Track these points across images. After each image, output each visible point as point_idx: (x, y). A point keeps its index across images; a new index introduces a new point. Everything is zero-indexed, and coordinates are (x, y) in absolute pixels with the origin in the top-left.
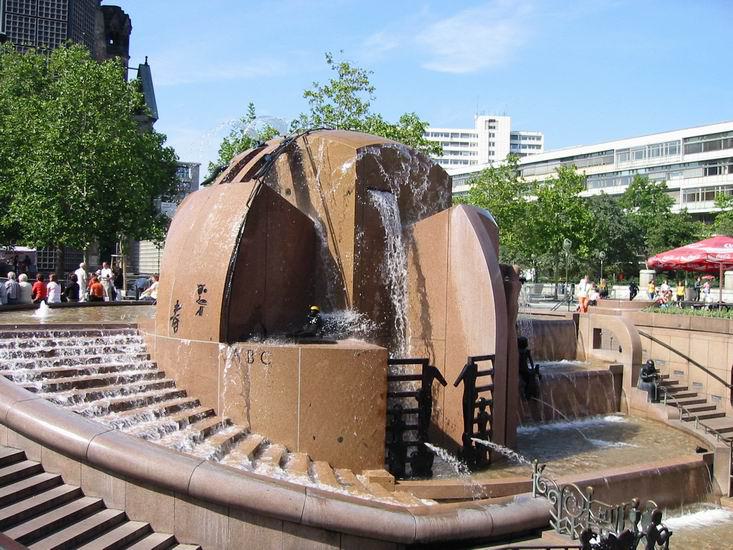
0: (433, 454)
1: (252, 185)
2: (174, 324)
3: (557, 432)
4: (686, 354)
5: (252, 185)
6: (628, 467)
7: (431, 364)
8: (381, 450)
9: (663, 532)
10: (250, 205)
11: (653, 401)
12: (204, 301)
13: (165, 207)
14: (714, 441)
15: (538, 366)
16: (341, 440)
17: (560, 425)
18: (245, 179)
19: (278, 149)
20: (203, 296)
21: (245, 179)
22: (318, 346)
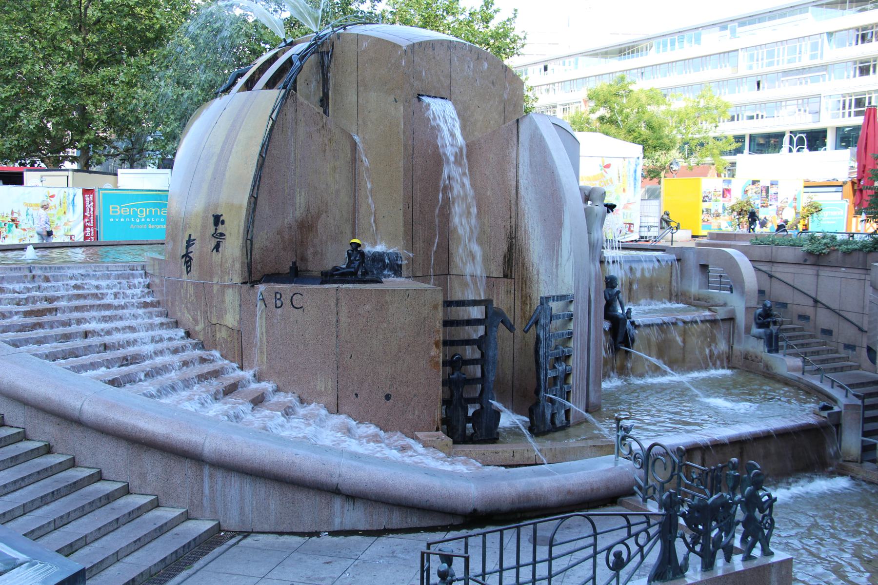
0: (492, 404)
1: (275, 94)
2: (186, 262)
3: (652, 387)
4: (791, 283)
5: (275, 94)
6: (737, 426)
7: (495, 305)
8: (439, 412)
9: (766, 498)
11: (769, 351)
12: (222, 234)
13: (709, 443)
14: (842, 399)
15: (629, 309)
16: (388, 397)
17: (650, 380)
18: (270, 85)
19: (307, 49)
20: (221, 228)
21: (270, 85)
22: (358, 286)
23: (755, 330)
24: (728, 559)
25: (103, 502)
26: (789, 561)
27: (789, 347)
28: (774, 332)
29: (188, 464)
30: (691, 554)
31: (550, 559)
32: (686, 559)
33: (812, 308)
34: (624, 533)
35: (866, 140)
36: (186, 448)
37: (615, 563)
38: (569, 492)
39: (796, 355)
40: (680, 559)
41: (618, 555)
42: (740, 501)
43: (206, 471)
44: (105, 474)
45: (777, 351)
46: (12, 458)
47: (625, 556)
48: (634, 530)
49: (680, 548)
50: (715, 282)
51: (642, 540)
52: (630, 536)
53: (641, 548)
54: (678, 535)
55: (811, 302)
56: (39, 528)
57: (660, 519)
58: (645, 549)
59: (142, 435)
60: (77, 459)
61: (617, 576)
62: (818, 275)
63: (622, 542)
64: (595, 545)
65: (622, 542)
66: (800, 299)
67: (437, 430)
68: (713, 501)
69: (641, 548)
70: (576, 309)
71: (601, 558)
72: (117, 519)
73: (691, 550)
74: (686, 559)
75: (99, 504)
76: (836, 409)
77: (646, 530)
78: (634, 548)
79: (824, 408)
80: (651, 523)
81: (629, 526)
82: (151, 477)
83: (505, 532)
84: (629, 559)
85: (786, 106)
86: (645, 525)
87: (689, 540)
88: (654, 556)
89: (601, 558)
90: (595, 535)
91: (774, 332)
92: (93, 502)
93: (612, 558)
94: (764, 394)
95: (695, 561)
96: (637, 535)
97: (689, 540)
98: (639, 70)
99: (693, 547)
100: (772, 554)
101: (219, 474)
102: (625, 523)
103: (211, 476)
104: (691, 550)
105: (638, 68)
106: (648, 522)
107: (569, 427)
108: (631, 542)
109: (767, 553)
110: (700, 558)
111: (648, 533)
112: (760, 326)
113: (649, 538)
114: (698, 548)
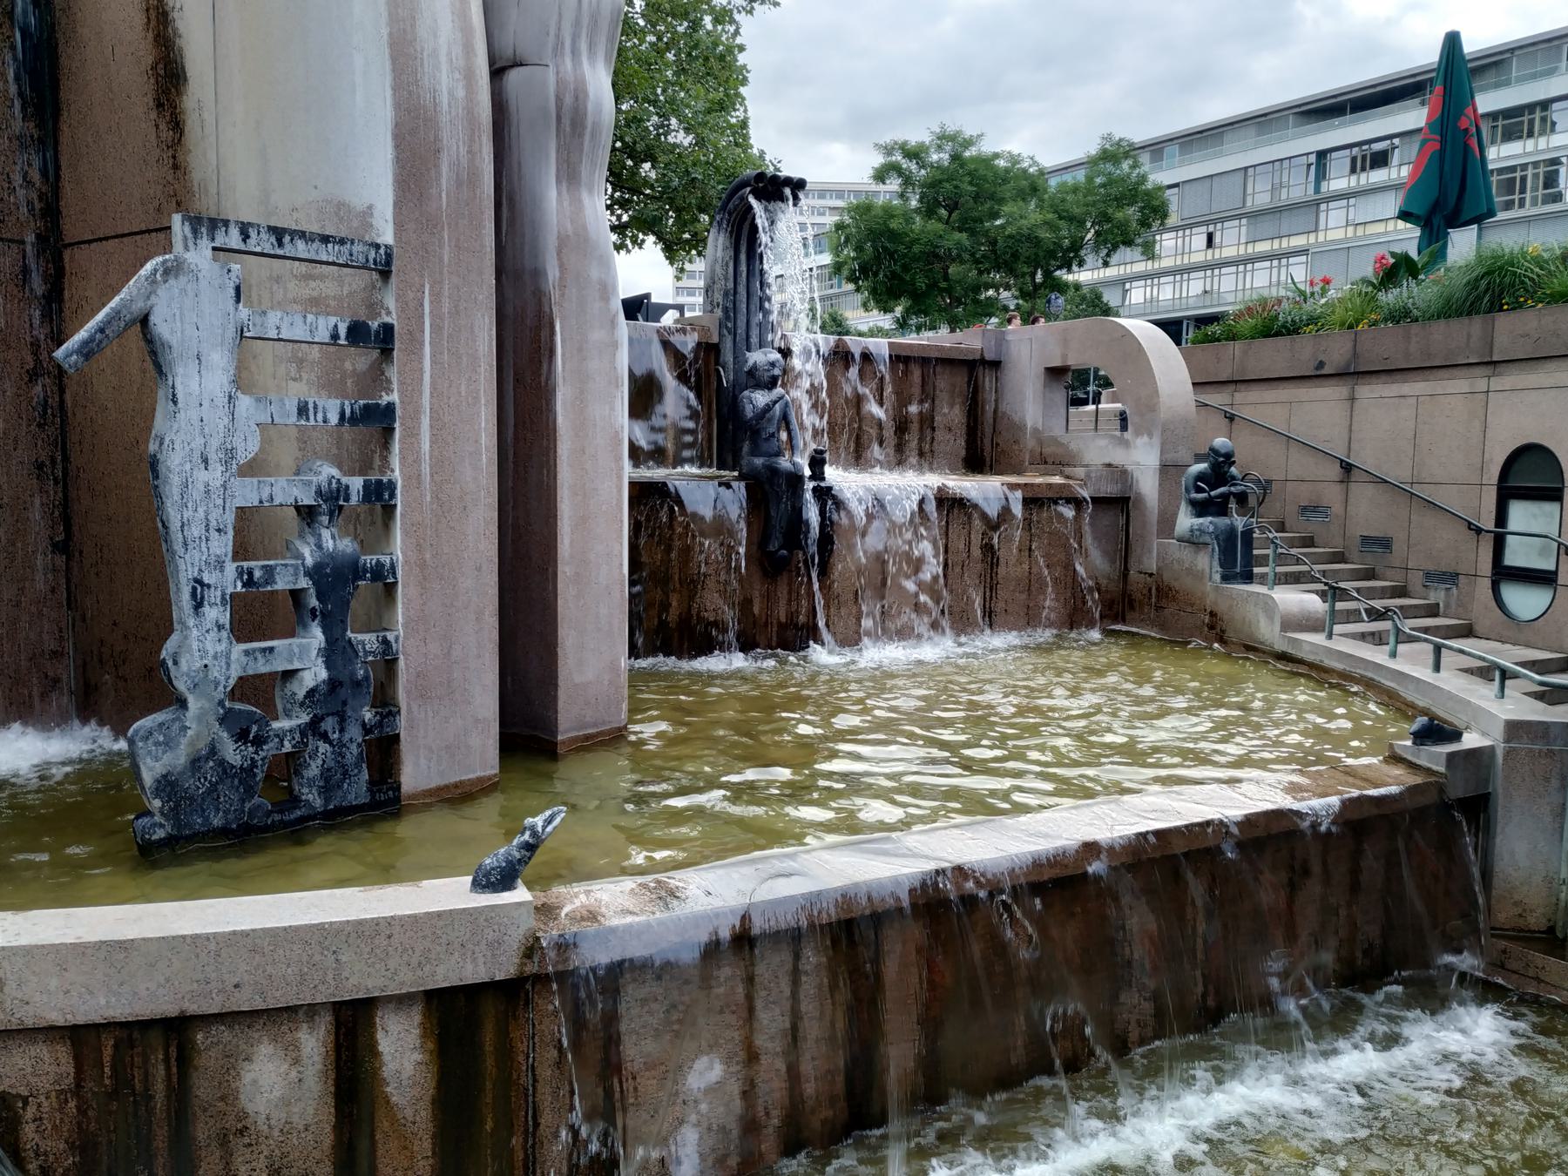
11: (1226, 578)
23: (1186, 521)
45: (1248, 577)
55: (1335, 471)
66: (1300, 465)
76: (1470, 740)
112: (1200, 509)
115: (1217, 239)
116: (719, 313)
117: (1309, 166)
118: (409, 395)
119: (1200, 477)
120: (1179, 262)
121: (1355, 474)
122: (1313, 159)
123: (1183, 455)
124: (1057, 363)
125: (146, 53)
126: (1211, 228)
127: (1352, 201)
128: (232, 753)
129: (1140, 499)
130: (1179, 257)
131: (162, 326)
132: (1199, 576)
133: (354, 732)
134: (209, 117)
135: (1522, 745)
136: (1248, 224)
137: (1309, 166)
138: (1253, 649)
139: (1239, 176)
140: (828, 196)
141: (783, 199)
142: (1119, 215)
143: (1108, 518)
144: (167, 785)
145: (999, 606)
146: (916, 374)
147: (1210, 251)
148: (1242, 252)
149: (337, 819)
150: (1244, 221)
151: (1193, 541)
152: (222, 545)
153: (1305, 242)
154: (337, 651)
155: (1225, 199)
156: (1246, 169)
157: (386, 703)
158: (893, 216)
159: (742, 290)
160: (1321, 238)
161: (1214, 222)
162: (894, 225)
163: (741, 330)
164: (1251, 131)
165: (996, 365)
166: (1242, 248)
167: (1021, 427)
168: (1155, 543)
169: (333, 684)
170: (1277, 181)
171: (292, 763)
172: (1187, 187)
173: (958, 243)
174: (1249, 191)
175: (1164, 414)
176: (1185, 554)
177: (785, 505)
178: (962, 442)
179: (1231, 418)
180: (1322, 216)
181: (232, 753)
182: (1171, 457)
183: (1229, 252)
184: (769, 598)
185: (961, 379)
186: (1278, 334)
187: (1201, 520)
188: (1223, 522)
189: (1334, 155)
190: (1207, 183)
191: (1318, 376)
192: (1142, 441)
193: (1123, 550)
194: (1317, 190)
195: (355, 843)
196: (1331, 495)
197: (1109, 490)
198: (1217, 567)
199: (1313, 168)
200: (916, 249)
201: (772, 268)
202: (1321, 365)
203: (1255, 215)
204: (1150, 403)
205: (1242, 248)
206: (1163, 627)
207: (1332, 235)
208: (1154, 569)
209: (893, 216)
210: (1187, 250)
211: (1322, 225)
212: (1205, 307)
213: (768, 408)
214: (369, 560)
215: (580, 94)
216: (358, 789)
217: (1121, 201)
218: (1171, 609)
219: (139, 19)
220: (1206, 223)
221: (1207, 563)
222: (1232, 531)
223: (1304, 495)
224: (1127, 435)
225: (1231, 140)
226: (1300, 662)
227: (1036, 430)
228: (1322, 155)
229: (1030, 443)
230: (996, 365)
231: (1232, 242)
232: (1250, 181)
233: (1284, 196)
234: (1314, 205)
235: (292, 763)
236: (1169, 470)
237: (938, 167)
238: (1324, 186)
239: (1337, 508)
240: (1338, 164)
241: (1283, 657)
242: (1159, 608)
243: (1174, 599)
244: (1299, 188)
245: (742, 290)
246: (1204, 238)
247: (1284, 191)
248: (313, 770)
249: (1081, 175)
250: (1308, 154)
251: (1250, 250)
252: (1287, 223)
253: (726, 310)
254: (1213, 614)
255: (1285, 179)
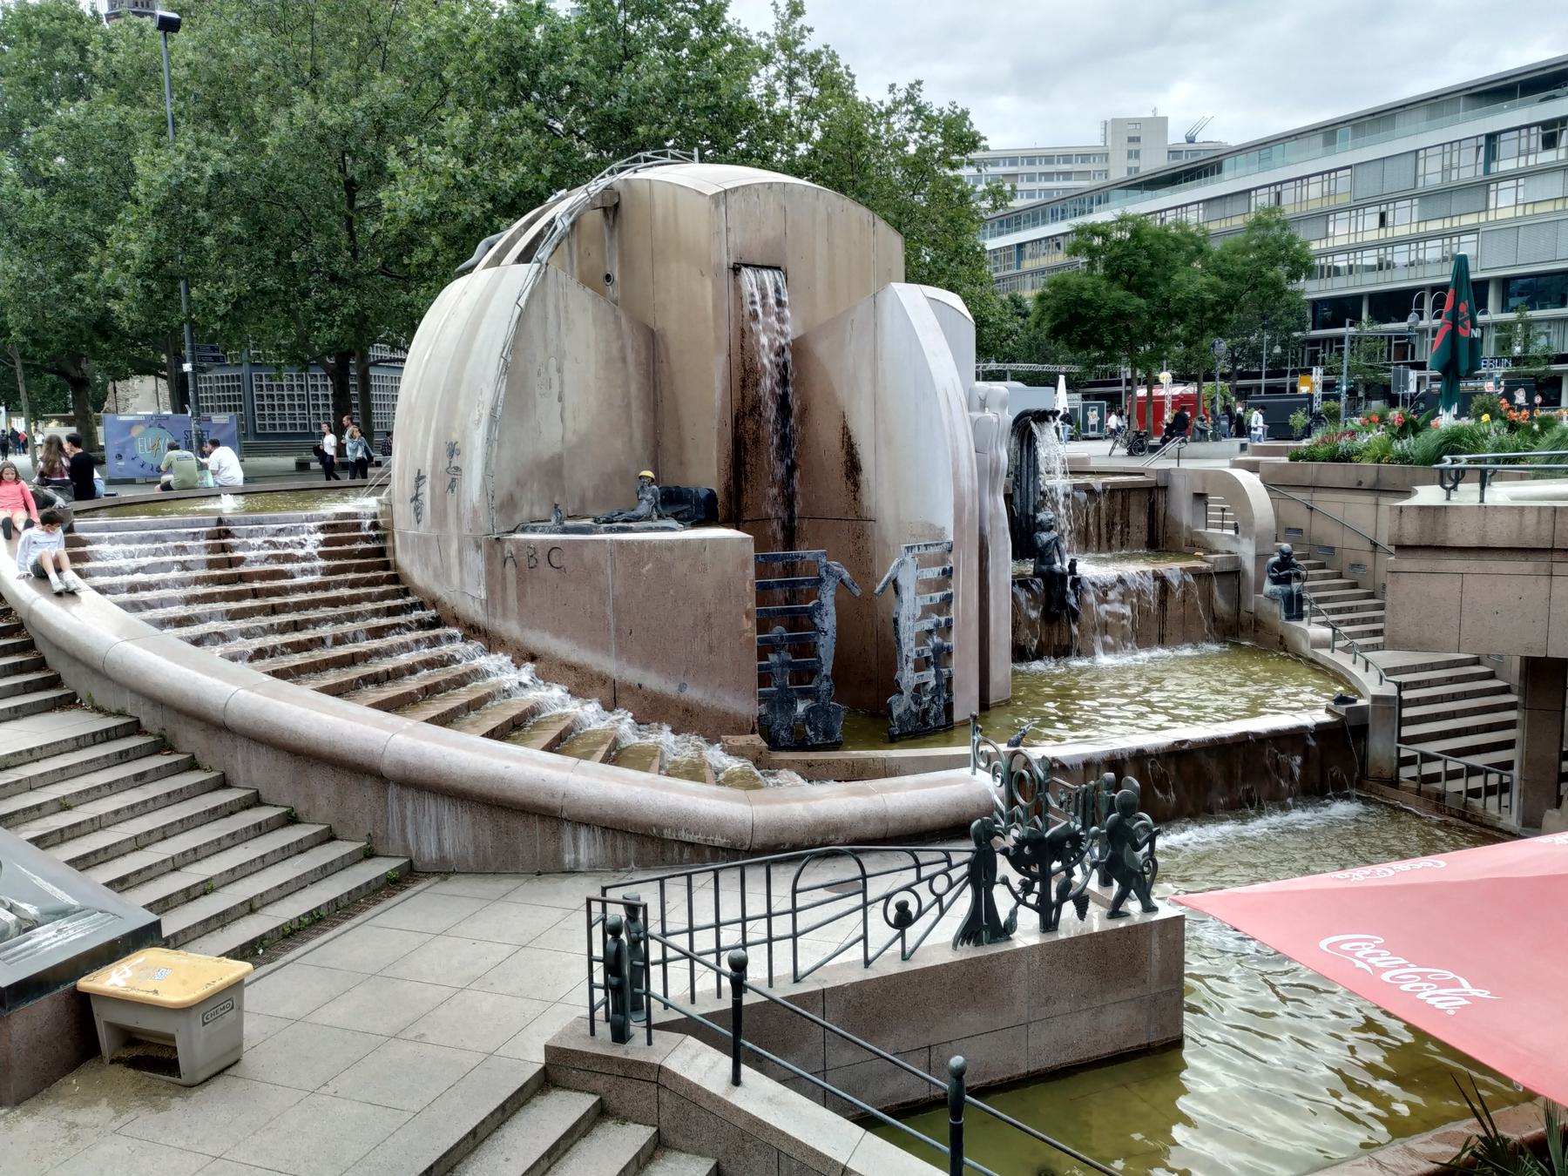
2: (416, 509)
10: (522, 302)
11: (1288, 618)
12: (457, 469)
20: (456, 462)
23: (1268, 587)
24: (1082, 912)
25: (252, 833)
26: (1179, 920)
27: (1318, 613)
28: (1295, 591)
29: (368, 782)
30: (1021, 908)
31: (794, 911)
32: (1013, 913)
33: (1370, 554)
34: (911, 876)
35: (178, 499)
36: (359, 760)
37: (898, 918)
38: (919, 820)
39: (1324, 624)
40: (1003, 916)
41: (902, 907)
42: (1095, 836)
43: (393, 791)
44: (264, 795)
45: (1300, 617)
46: (139, 774)
47: (913, 908)
48: (925, 872)
49: (1003, 901)
50: (1215, 517)
51: (941, 884)
52: (919, 880)
53: (939, 898)
54: (998, 879)
55: (1368, 546)
56: (149, 868)
57: (968, 856)
58: (946, 900)
59: (302, 744)
60: (228, 775)
61: (902, 935)
62: (1377, 505)
63: (908, 888)
64: (864, 892)
65: (908, 888)
66: (1350, 541)
67: (753, 732)
68: (1053, 834)
69: (939, 898)
70: (957, 561)
71: (875, 912)
72: (263, 857)
73: (1021, 902)
74: (1013, 913)
75: (244, 836)
76: (1361, 702)
77: (945, 872)
78: (928, 899)
79: (1341, 700)
80: (954, 863)
81: (918, 866)
82: (321, 801)
83: (722, 875)
84: (920, 913)
85: (1459, 244)
86: (945, 865)
87: (1017, 887)
88: (962, 906)
89: (875, 912)
90: (864, 877)
91: (1295, 591)
92: (235, 833)
93: (892, 913)
94: (1126, 686)
95: (1028, 920)
96: (931, 878)
97: (1017, 887)
98: (1272, 188)
99: (1024, 898)
100: (1155, 909)
101: (409, 795)
102: (912, 862)
103: (400, 799)
104: (1021, 902)
105: (1269, 186)
106: (948, 860)
107: (952, 729)
108: (922, 889)
109: (1149, 908)
110: (1037, 915)
111: (950, 878)
112: (1276, 581)
113: (951, 885)
114: (1032, 899)
115: (1390, 218)
116: (1012, 477)
117: (1478, 148)
118: (957, 589)
119: (1275, 565)
120: (1352, 241)
121: (1379, 549)
122: (1482, 141)
123: (1268, 549)
124: (1200, 491)
125: (842, 456)
126: (1384, 208)
127: (1521, 181)
128: (914, 708)
129: (1245, 573)
130: (1352, 237)
131: (901, 581)
132: (1275, 616)
133: (942, 701)
134: (872, 484)
135: (1379, 705)
136: (1420, 205)
137: (1478, 148)
138: (1298, 657)
139: (1412, 158)
140: (1001, 163)
141: (1048, 420)
142: (1271, 274)
143: (1226, 582)
144: (899, 717)
145: (1167, 632)
146: (1119, 496)
147: (1382, 230)
148: (1414, 230)
149: (935, 731)
150: (1416, 201)
151: (1272, 597)
152: (912, 644)
153: (1475, 221)
154: (938, 675)
155: (1398, 179)
156: (1417, 151)
157: (949, 691)
158: (1085, 289)
159: (1025, 464)
160: (1491, 218)
161: (1387, 202)
162: (1086, 295)
163: (1024, 486)
164: (1422, 114)
165: (1165, 488)
166: (1414, 226)
167: (1180, 525)
168: (1254, 596)
169: (937, 685)
170: (1447, 162)
171: (926, 712)
172: (1359, 168)
173: (1138, 307)
174: (1421, 171)
175: (1257, 528)
176: (1267, 604)
177: (1058, 589)
178: (1145, 533)
179: (1312, 509)
180: (1492, 195)
181: (914, 708)
182: (1261, 551)
183: (1401, 231)
184: (1049, 634)
185: (1145, 497)
186: (1338, 460)
187: (1275, 587)
188: (1286, 588)
189: (1503, 137)
190: (1379, 165)
191: (1358, 488)
192: (1246, 541)
193: (1237, 599)
194: (1487, 171)
195: (942, 737)
196: (1367, 558)
197: (1228, 567)
198: (1283, 613)
199: (1482, 149)
200: (1103, 313)
201: (1042, 453)
202: (1360, 483)
203: (1427, 196)
204: (1250, 520)
205: (1414, 226)
206: (1256, 640)
207: (1501, 215)
208: (1253, 610)
209: (1085, 289)
210: (1360, 229)
211: (1492, 205)
212: (1378, 284)
213: (1049, 543)
214: (946, 644)
215: (998, 458)
216: (943, 721)
217: (1273, 261)
218: (1261, 632)
219: (838, 444)
220: (1379, 204)
221: (1278, 610)
222: (1291, 593)
223: (1352, 558)
224: (1238, 536)
225: (1403, 123)
226: (1318, 664)
227: (1188, 527)
228: (1492, 138)
229: (1185, 534)
230: (1165, 488)
231: (1404, 221)
232: (1421, 163)
233: (1454, 178)
234: (1482, 187)
235: (926, 712)
236: (1260, 557)
237: (1119, 242)
238: (1494, 167)
239: (1370, 566)
240: (1506, 146)
241: (1312, 661)
242: (1256, 631)
243: (1263, 627)
244: (1469, 168)
245: (1025, 464)
246: (1377, 218)
247: (1454, 172)
248: (932, 714)
249: (1240, 236)
250: (1477, 137)
251: (1422, 229)
252: (1457, 203)
253: (1016, 476)
254: (1281, 637)
255: (1455, 161)
